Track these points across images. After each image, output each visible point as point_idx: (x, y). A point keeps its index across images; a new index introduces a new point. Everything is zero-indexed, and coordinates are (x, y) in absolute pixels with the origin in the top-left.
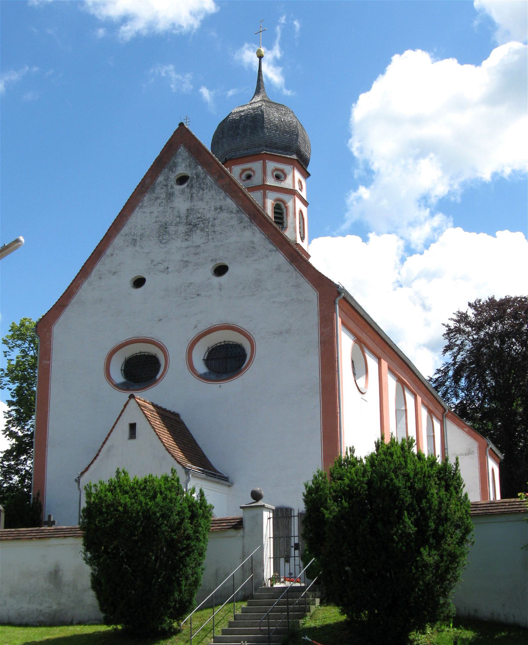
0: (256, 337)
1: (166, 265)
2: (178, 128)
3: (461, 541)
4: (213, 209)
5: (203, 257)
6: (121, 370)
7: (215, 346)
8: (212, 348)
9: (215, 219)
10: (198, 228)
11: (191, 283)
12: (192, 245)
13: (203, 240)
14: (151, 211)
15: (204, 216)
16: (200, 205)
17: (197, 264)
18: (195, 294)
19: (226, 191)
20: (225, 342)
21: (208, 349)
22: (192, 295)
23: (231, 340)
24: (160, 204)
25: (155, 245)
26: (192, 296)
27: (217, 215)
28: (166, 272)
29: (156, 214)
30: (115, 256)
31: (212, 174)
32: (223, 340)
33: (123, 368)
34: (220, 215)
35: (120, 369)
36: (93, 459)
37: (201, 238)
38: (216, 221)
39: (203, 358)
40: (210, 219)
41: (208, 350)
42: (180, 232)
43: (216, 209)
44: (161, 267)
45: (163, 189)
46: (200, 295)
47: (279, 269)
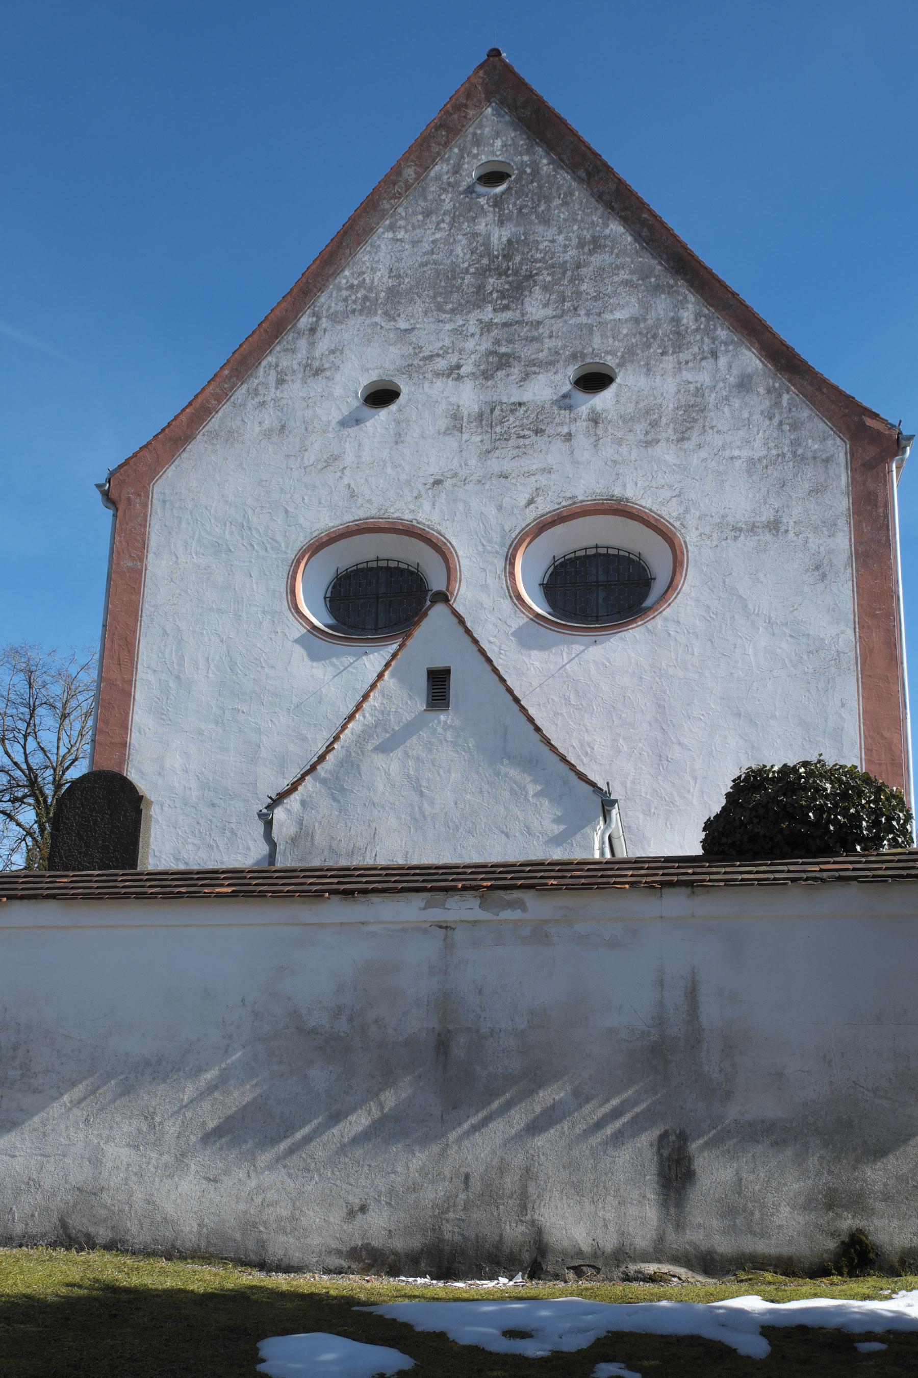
0: (690, 538)
1: (454, 359)
2: (486, 61)
3: (773, 534)
4: (575, 241)
5: (549, 349)
6: (325, 598)
7: (563, 559)
8: (555, 567)
9: (578, 266)
10: (536, 282)
11: (520, 404)
12: (521, 319)
13: (549, 312)
14: (416, 239)
15: (552, 258)
16: (545, 235)
17: (533, 363)
18: (529, 429)
19: (609, 206)
20: (597, 547)
21: (555, 562)
22: (523, 430)
23: (610, 543)
24: (438, 224)
25: (426, 314)
26: (522, 433)
27: (585, 257)
28: (455, 376)
29: (426, 246)
30: (319, 333)
31: (573, 168)
32: (592, 543)
33: (329, 595)
34: (592, 259)
35: (323, 596)
36: (315, 759)
37: (545, 305)
38: (584, 271)
39: (539, 581)
40: (568, 265)
41: (554, 564)
42: (489, 288)
43: (581, 245)
44: (441, 364)
45: (448, 191)
46: (543, 431)
47: (744, 384)
